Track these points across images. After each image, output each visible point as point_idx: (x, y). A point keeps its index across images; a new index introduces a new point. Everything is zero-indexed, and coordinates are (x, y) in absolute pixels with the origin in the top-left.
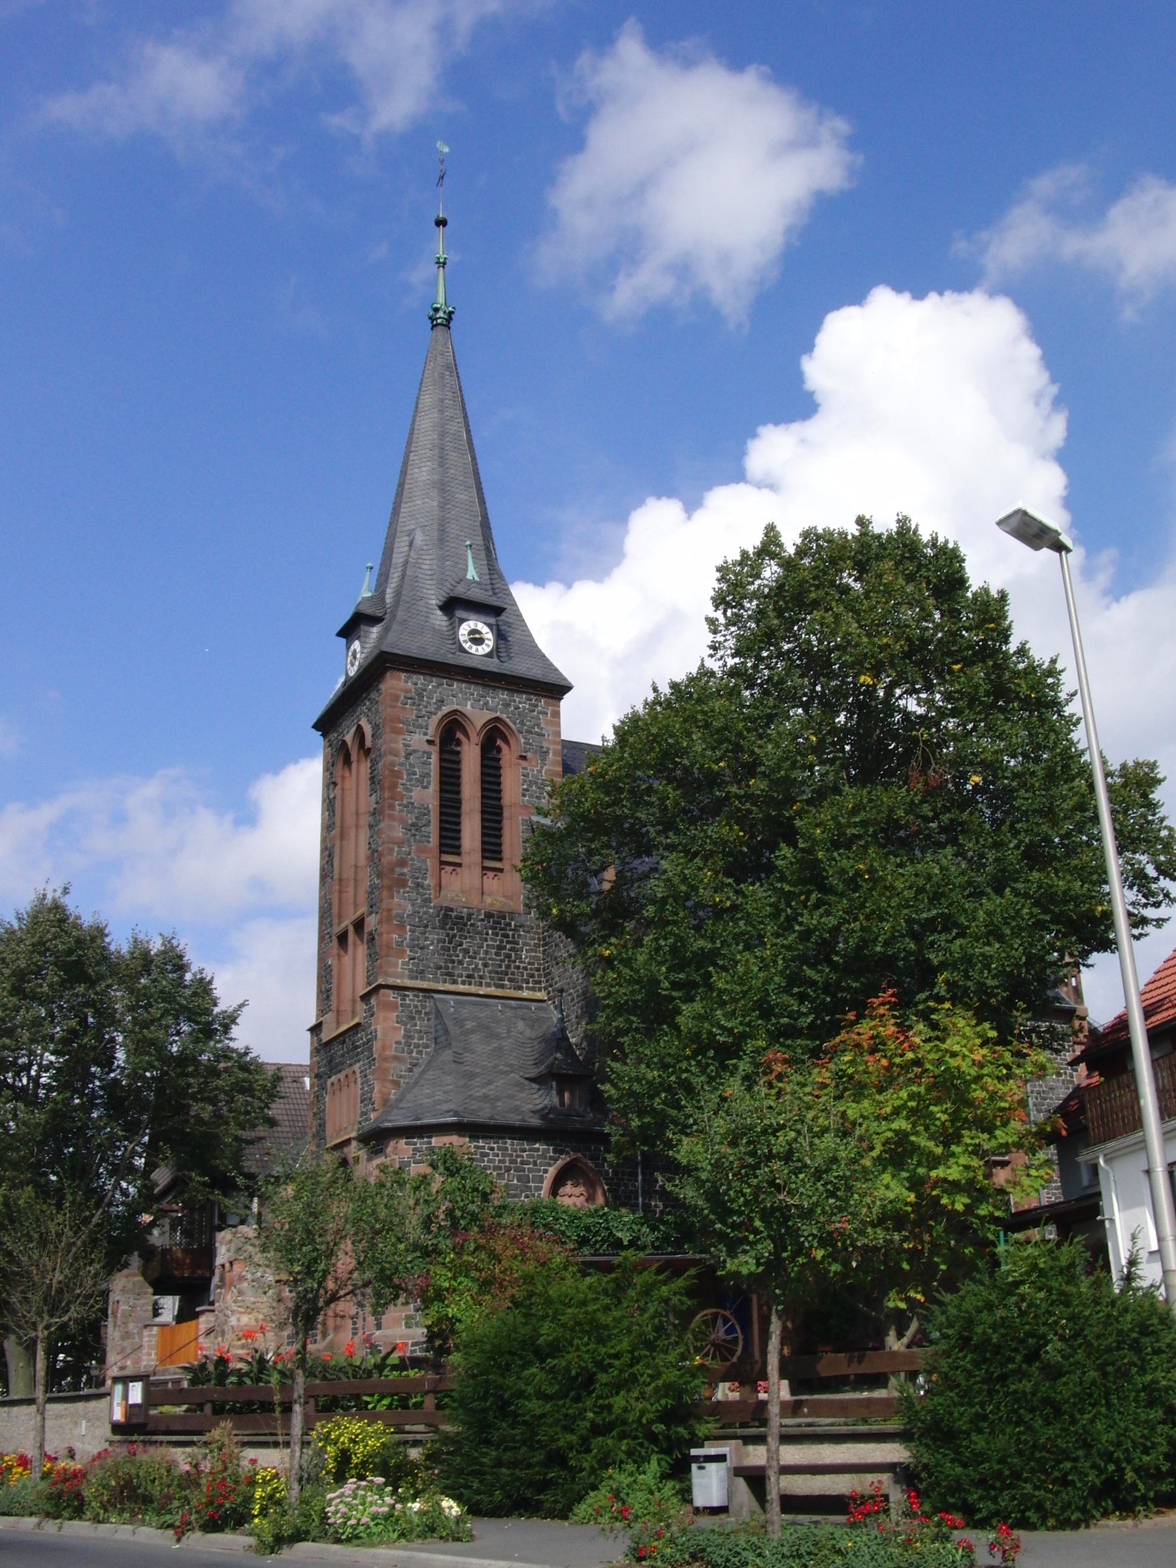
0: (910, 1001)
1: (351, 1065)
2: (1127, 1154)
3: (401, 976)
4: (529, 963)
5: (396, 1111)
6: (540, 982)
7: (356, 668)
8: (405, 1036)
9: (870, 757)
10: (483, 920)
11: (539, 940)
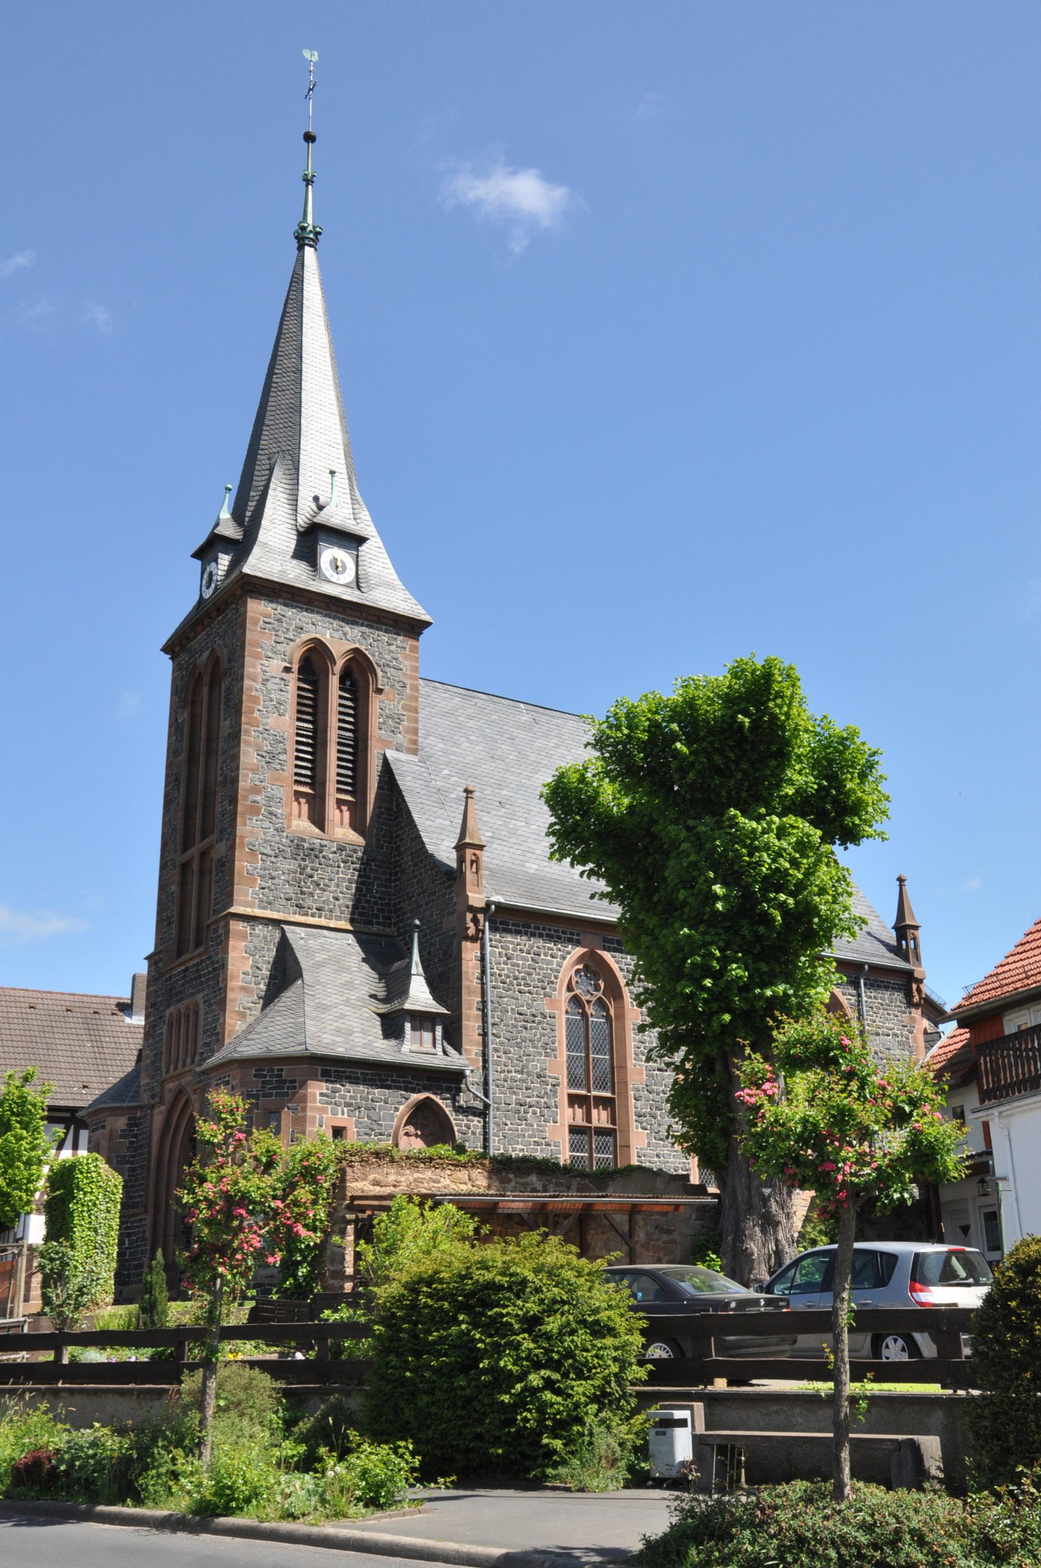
1: (193, 994)
2: (1025, 1111)
3: (251, 905)
4: (380, 898)
5: (245, 1042)
6: (390, 918)
7: (211, 590)
10: (335, 853)
11: (391, 875)
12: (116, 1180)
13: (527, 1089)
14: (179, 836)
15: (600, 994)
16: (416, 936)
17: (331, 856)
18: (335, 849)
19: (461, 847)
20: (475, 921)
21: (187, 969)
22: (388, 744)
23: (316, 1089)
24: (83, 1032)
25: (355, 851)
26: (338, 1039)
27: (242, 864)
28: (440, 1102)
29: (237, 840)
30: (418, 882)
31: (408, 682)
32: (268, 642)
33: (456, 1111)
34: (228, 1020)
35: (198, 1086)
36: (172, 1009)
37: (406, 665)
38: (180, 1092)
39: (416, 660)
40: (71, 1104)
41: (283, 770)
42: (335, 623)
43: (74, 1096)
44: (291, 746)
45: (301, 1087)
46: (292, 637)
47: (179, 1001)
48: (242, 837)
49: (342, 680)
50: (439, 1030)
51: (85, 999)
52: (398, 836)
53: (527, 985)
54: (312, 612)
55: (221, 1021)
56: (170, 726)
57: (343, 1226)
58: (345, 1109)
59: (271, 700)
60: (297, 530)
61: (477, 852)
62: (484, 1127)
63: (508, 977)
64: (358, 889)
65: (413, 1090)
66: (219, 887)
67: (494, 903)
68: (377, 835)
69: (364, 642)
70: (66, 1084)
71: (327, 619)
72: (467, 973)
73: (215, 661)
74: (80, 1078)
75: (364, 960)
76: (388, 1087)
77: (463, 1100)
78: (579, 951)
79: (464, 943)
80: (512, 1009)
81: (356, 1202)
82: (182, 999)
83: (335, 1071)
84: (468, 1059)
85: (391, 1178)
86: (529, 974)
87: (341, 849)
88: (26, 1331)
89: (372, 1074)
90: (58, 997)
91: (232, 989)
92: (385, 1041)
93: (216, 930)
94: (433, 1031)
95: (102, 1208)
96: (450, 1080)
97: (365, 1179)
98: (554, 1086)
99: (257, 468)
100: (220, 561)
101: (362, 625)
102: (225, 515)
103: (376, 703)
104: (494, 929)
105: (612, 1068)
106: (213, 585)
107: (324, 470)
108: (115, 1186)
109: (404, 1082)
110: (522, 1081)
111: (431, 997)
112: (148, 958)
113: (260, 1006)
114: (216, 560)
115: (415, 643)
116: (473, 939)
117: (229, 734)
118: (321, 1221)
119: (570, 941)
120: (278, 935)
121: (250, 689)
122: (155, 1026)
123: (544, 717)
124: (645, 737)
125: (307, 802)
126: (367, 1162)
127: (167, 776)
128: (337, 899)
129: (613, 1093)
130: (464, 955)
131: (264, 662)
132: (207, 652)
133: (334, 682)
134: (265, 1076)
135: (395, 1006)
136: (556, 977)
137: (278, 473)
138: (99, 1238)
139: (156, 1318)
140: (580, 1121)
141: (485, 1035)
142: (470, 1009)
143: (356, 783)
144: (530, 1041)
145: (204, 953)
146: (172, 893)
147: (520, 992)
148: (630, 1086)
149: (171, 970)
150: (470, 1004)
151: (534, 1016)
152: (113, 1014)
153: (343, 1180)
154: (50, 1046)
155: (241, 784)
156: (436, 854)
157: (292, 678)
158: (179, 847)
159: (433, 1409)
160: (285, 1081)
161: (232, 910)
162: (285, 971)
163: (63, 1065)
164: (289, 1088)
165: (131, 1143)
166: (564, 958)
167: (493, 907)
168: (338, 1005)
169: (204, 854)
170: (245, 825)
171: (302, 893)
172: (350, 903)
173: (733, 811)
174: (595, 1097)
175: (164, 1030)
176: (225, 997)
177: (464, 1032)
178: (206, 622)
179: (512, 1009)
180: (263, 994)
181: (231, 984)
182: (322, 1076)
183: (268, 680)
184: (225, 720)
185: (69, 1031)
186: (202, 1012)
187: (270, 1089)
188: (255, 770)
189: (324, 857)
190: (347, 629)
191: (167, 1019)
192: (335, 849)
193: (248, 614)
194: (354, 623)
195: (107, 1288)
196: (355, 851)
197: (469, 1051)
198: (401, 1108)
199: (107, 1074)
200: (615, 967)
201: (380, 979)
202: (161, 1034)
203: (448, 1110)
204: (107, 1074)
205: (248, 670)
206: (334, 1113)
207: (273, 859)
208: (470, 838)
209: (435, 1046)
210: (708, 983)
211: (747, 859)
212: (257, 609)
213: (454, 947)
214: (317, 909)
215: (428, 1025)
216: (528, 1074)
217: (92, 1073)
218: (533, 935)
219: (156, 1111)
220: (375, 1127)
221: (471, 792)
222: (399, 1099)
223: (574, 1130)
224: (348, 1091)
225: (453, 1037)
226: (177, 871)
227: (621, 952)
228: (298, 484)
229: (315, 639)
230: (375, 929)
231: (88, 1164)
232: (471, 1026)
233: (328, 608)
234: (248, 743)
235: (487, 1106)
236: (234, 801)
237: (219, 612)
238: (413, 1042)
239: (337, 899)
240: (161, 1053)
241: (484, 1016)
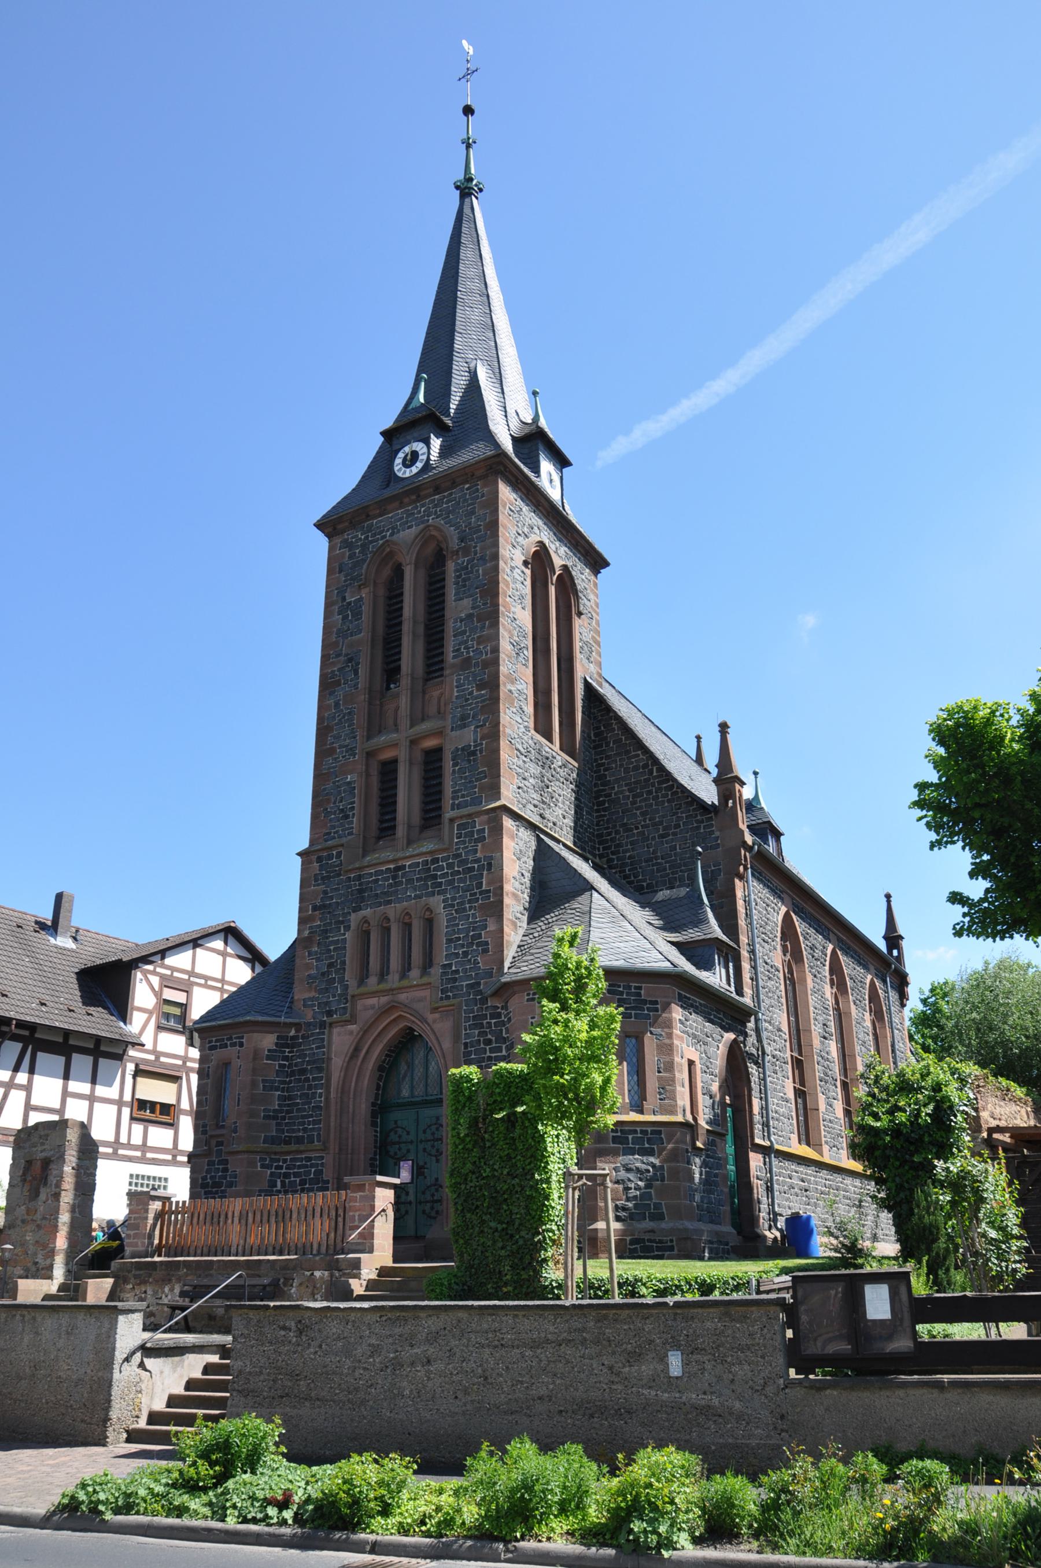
21: (398, 869)
36: (367, 912)
45: (664, 1010)
52: (603, 764)
55: (492, 927)
82: (389, 902)
103: (578, 623)
116: (741, 878)
122: (326, 931)
134: (622, 993)
152: (36, 931)
160: (645, 1002)
165: (280, 1065)
237: (437, 490)
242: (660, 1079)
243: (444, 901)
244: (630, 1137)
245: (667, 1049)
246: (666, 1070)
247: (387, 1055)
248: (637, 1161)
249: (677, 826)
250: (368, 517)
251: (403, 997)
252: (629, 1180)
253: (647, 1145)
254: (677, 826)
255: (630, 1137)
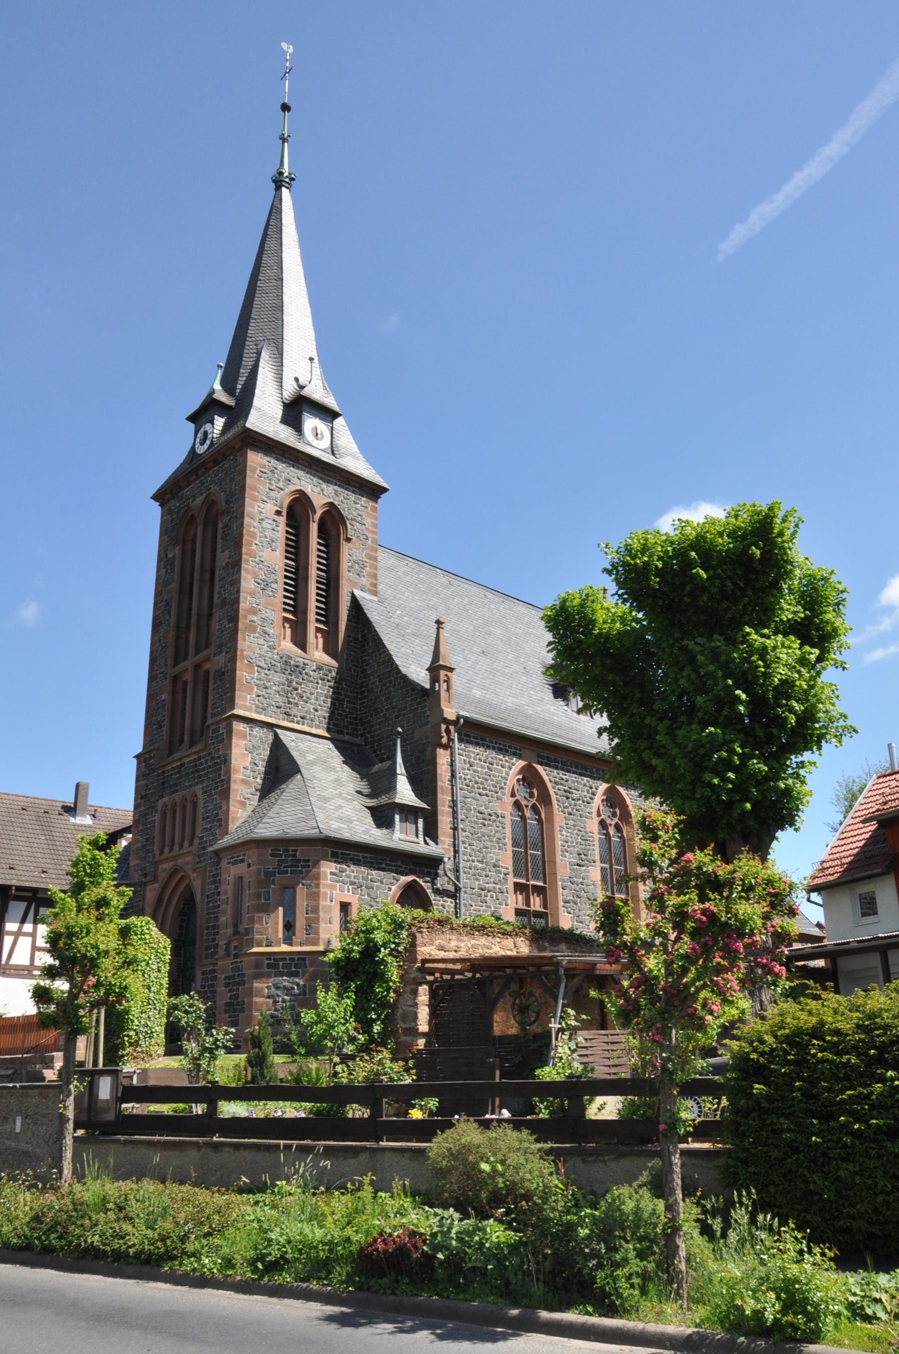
0: (737, 1092)
1: (190, 786)
3: (250, 710)
4: (349, 713)
6: (356, 730)
7: (206, 446)
8: (251, 762)
9: (735, 655)
10: (315, 671)
11: (357, 693)
12: (165, 943)
13: (486, 876)
14: (170, 652)
15: (534, 801)
16: (399, 741)
17: (312, 673)
18: (314, 668)
19: (435, 669)
20: (448, 731)
21: (182, 765)
22: (355, 585)
23: (328, 868)
24: (37, 827)
25: (330, 671)
26: (342, 826)
27: (242, 674)
28: (423, 884)
29: (238, 653)
30: (387, 700)
31: (369, 535)
32: (263, 489)
33: (434, 893)
34: (231, 808)
35: (199, 865)
36: (165, 799)
37: (368, 521)
38: (175, 871)
39: (376, 518)
40: (34, 885)
41: (274, 597)
42: (315, 480)
43: (36, 879)
44: (280, 576)
45: (314, 866)
46: (282, 486)
47: (173, 793)
48: (242, 650)
49: (320, 531)
50: (421, 822)
51: (36, 801)
52: (365, 661)
53: (484, 789)
54: (298, 468)
55: (224, 808)
56: (159, 561)
57: (414, 987)
58: (350, 887)
59: (266, 537)
60: (283, 402)
61: (448, 673)
62: (456, 908)
63: (471, 781)
64: (333, 704)
65: (402, 873)
66: (218, 693)
67: (463, 717)
68: (347, 660)
69: (336, 498)
70: (29, 869)
71: (309, 476)
72: (441, 775)
73: (210, 504)
74: (39, 865)
75: (344, 762)
76: (383, 870)
77: (440, 883)
78: (521, 763)
79: (438, 750)
80: (475, 809)
81: (427, 965)
82: (177, 791)
83: (342, 853)
84: (443, 849)
85: (453, 944)
86: (486, 780)
87: (320, 668)
88: (135, 1082)
89: (371, 858)
90: (14, 798)
91: (235, 781)
92: (378, 830)
93: (216, 730)
94: (416, 823)
95: (154, 967)
96: (428, 865)
97: (432, 944)
98: (505, 874)
99: (246, 351)
100: (215, 422)
101: (335, 485)
102: (217, 386)
103: (346, 550)
104: (461, 740)
105: (544, 862)
106: (208, 442)
107: (299, 358)
108: (165, 948)
109: (395, 866)
110: (483, 869)
111: (412, 794)
112: (137, 757)
113: (257, 797)
114: (212, 422)
115: (375, 505)
116: (446, 747)
117: (227, 564)
118: (394, 982)
119: (515, 754)
120: (271, 737)
121: (249, 525)
122: (146, 815)
123: (456, 582)
124: (660, 564)
125: (291, 627)
126: (432, 928)
127: (156, 603)
128: (316, 710)
129: (545, 883)
130: (438, 760)
131: (260, 504)
132: (202, 498)
133: (314, 528)
135: (384, 800)
136: (505, 784)
137: (265, 355)
138: (152, 995)
139: (266, 1071)
140: (521, 906)
141: (455, 829)
142: (444, 806)
143: (329, 614)
144: (488, 836)
145: (203, 750)
146: (163, 701)
147: (480, 794)
148: (559, 878)
149: (164, 766)
150: (444, 802)
151: (490, 815)
152: (60, 814)
153: (413, 944)
154: (12, 837)
155: (242, 605)
156: (408, 675)
157: (282, 520)
158: (170, 661)
159: (858, 1179)
160: (299, 861)
161: (235, 712)
162: (280, 769)
163: (24, 853)
164: (302, 866)
166: (510, 768)
167: (462, 720)
168: (332, 797)
169: (197, 667)
170: (244, 640)
171: (289, 703)
172: (327, 715)
173: (748, 629)
174: (533, 886)
175: (157, 817)
176: (229, 788)
177: (439, 826)
178: (200, 473)
179: (475, 809)
180: (259, 787)
181: (234, 776)
182: (332, 857)
183: (263, 520)
184: (223, 551)
185: (26, 826)
186: (201, 804)
187: (285, 867)
188: (253, 594)
189: (306, 674)
190: (324, 486)
191: (159, 809)
192: (314, 668)
193: (249, 463)
194: (328, 482)
195: (159, 1041)
196: (330, 671)
197: (443, 842)
198: (393, 888)
199: (60, 862)
200: (546, 778)
201: (362, 778)
202: (153, 821)
203: (429, 891)
204: (60, 862)
205: (247, 509)
206: (342, 890)
207: (267, 672)
208: (444, 661)
209: (417, 837)
210: (731, 775)
211: (763, 670)
212: (255, 459)
213: (428, 753)
214: (302, 718)
215: (411, 818)
216: (487, 864)
217: (49, 861)
218: (488, 747)
219: (149, 888)
220: (373, 903)
221: (442, 623)
222: (392, 881)
223: (519, 912)
224: (354, 872)
225: (431, 832)
226: (168, 681)
227: (549, 766)
228: (282, 366)
229: (300, 490)
230: (346, 738)
231: (142, 926)
232: (444, 821)
233: (310, 467)
234: (247, 571)
235: (458, 889)
236: (234, 619)
237: (216, 462)
238: (401, 832)
239: (316, 710)
240: (154, 838)
241: (455, 813)
242: (307, 919)
243: (203, 789)
244: (281, 963)
245: (314, 896)
246: (312, 912)
247: (185, 904)
248: (285, 981)
249: (405, 708)
250: (181, 488)
251: (180, 862)
252: (278, 995)
253: (293, 969)
254: (405, 708)
255: (281, 963)
